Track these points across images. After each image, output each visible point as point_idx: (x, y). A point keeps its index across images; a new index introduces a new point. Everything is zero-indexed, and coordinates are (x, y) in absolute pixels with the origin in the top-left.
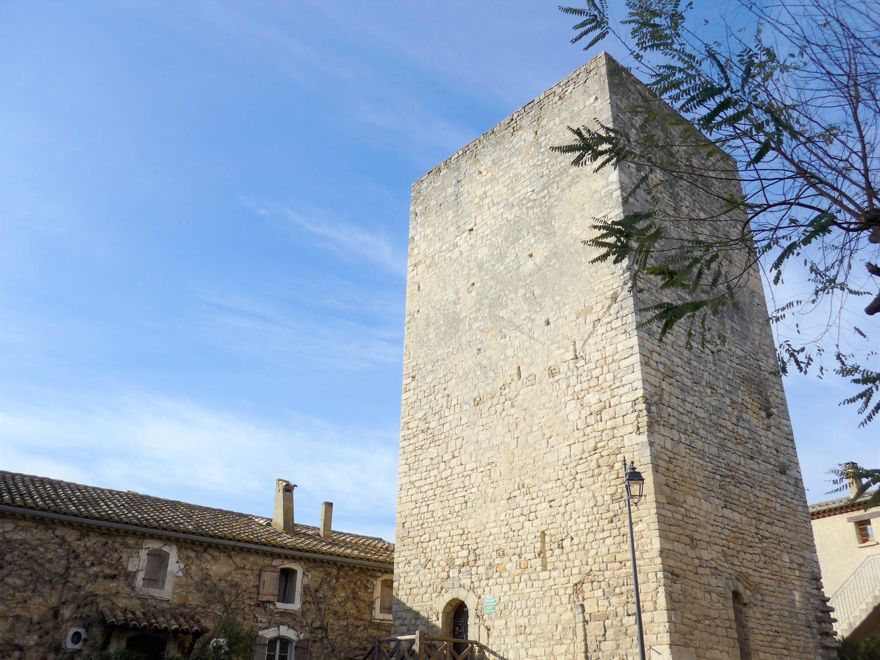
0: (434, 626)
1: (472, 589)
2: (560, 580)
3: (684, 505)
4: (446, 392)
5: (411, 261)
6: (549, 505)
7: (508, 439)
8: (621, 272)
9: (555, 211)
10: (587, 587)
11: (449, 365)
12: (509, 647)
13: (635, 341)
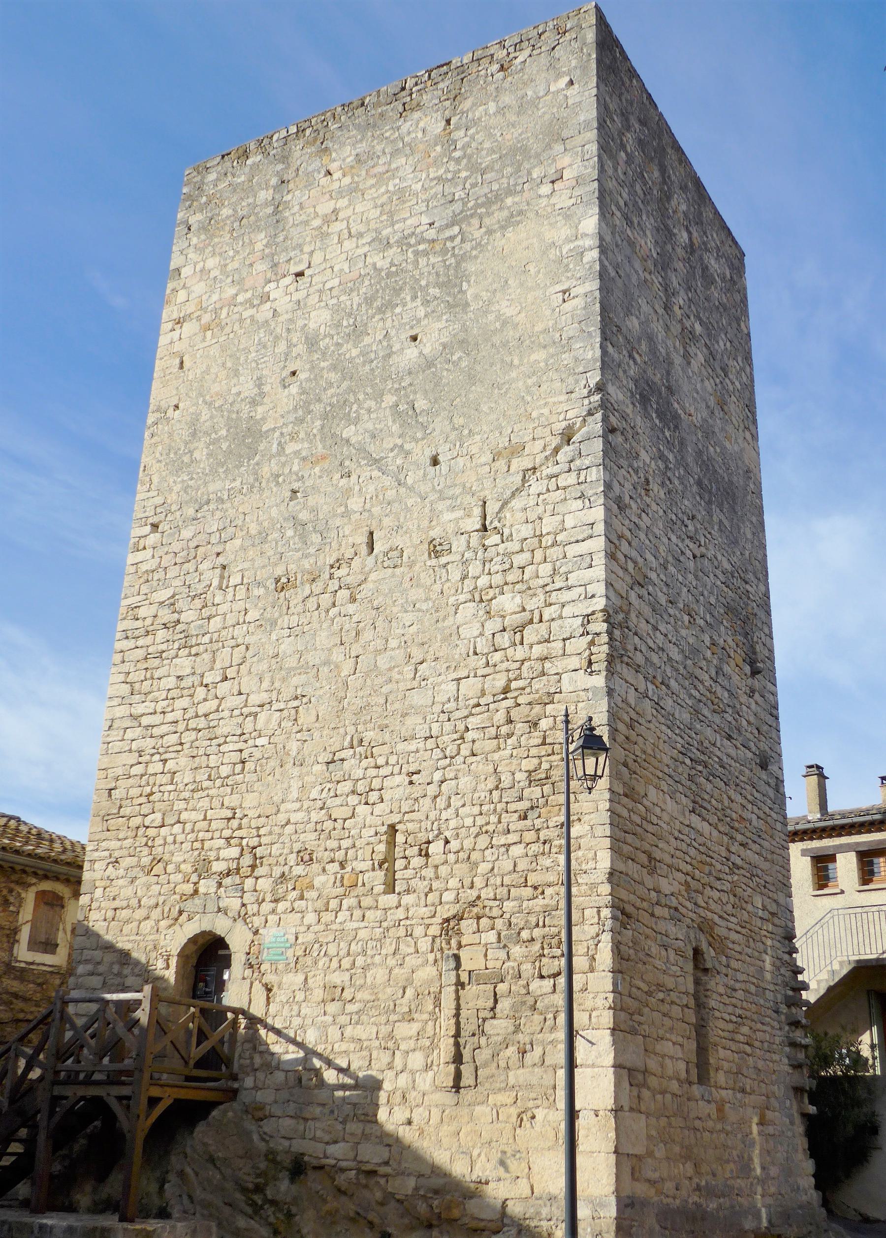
0: (161, 978)
1: (242, 917)
2: (417, 910)
3: (645, 801)
4: (221, 560)
5: (169, 313)
6: (407, 779)
7: (337, 656)
8: (585, 392)
9: (471, 267)
10: (468, 925)
11: (231, 512)
12: (308, 1021)
13: (598, 513)
